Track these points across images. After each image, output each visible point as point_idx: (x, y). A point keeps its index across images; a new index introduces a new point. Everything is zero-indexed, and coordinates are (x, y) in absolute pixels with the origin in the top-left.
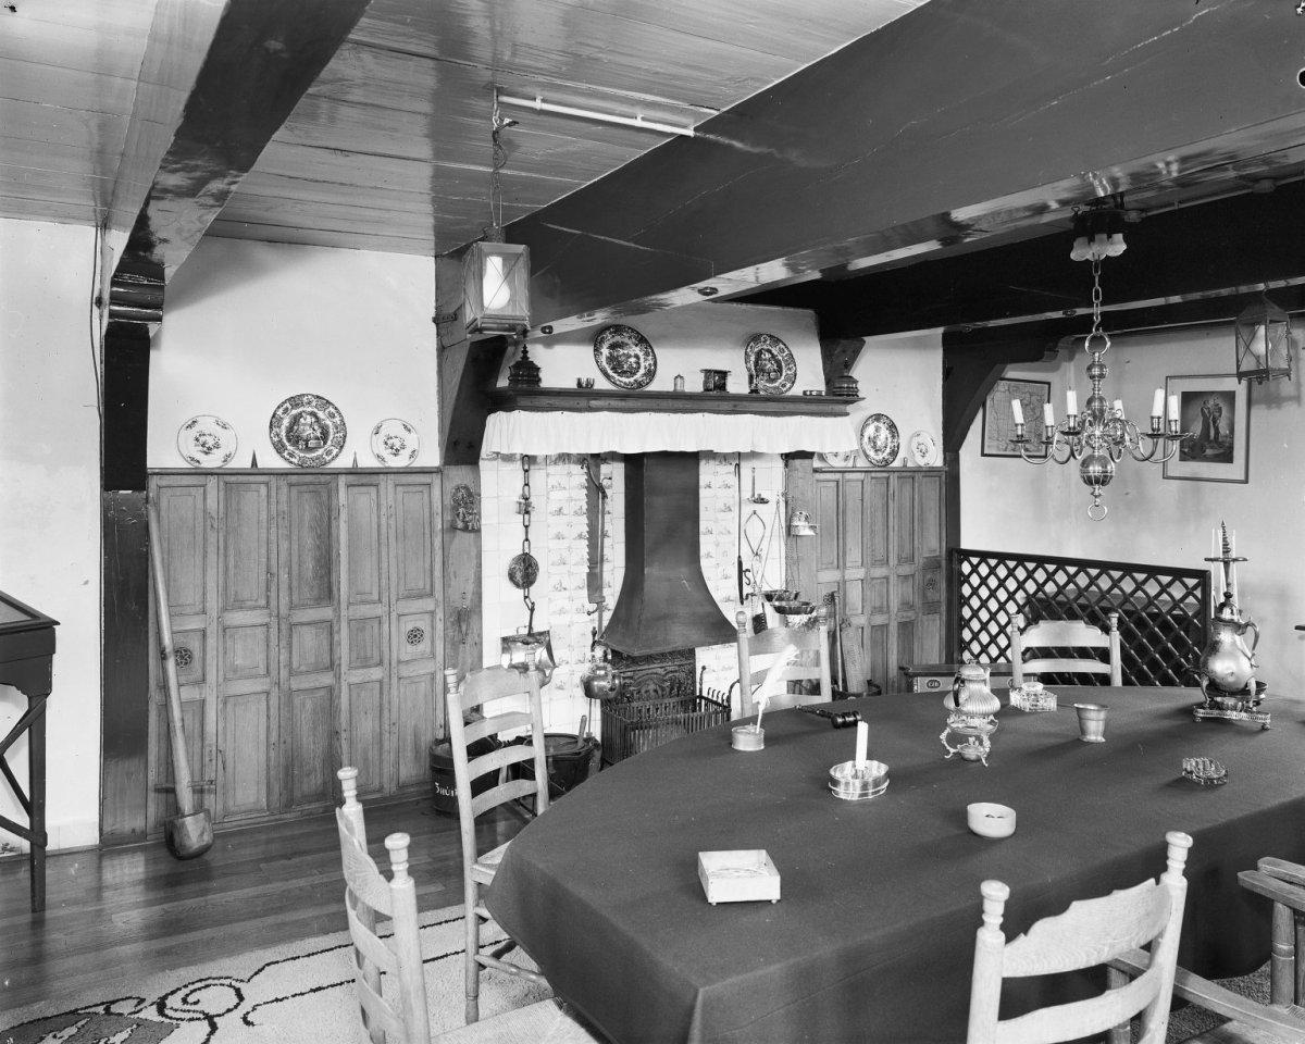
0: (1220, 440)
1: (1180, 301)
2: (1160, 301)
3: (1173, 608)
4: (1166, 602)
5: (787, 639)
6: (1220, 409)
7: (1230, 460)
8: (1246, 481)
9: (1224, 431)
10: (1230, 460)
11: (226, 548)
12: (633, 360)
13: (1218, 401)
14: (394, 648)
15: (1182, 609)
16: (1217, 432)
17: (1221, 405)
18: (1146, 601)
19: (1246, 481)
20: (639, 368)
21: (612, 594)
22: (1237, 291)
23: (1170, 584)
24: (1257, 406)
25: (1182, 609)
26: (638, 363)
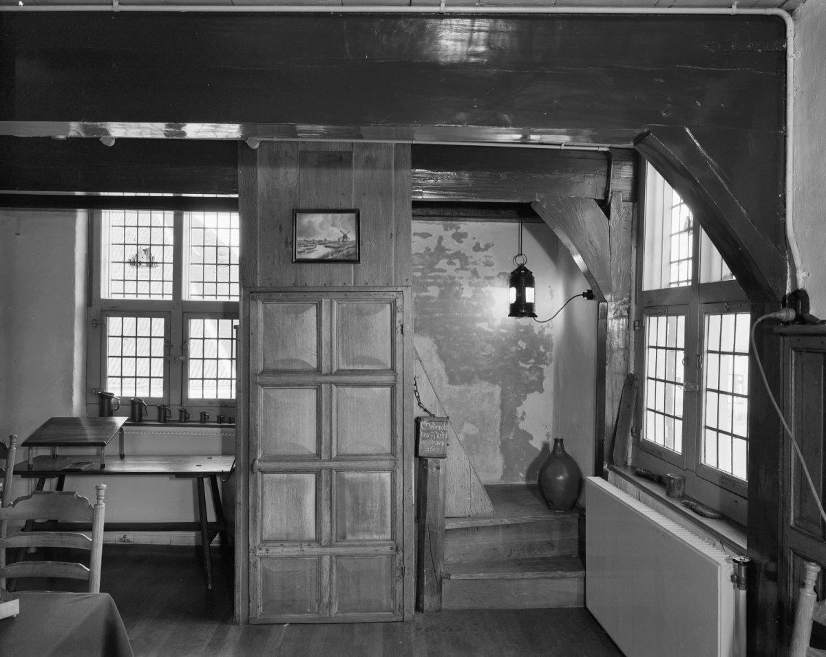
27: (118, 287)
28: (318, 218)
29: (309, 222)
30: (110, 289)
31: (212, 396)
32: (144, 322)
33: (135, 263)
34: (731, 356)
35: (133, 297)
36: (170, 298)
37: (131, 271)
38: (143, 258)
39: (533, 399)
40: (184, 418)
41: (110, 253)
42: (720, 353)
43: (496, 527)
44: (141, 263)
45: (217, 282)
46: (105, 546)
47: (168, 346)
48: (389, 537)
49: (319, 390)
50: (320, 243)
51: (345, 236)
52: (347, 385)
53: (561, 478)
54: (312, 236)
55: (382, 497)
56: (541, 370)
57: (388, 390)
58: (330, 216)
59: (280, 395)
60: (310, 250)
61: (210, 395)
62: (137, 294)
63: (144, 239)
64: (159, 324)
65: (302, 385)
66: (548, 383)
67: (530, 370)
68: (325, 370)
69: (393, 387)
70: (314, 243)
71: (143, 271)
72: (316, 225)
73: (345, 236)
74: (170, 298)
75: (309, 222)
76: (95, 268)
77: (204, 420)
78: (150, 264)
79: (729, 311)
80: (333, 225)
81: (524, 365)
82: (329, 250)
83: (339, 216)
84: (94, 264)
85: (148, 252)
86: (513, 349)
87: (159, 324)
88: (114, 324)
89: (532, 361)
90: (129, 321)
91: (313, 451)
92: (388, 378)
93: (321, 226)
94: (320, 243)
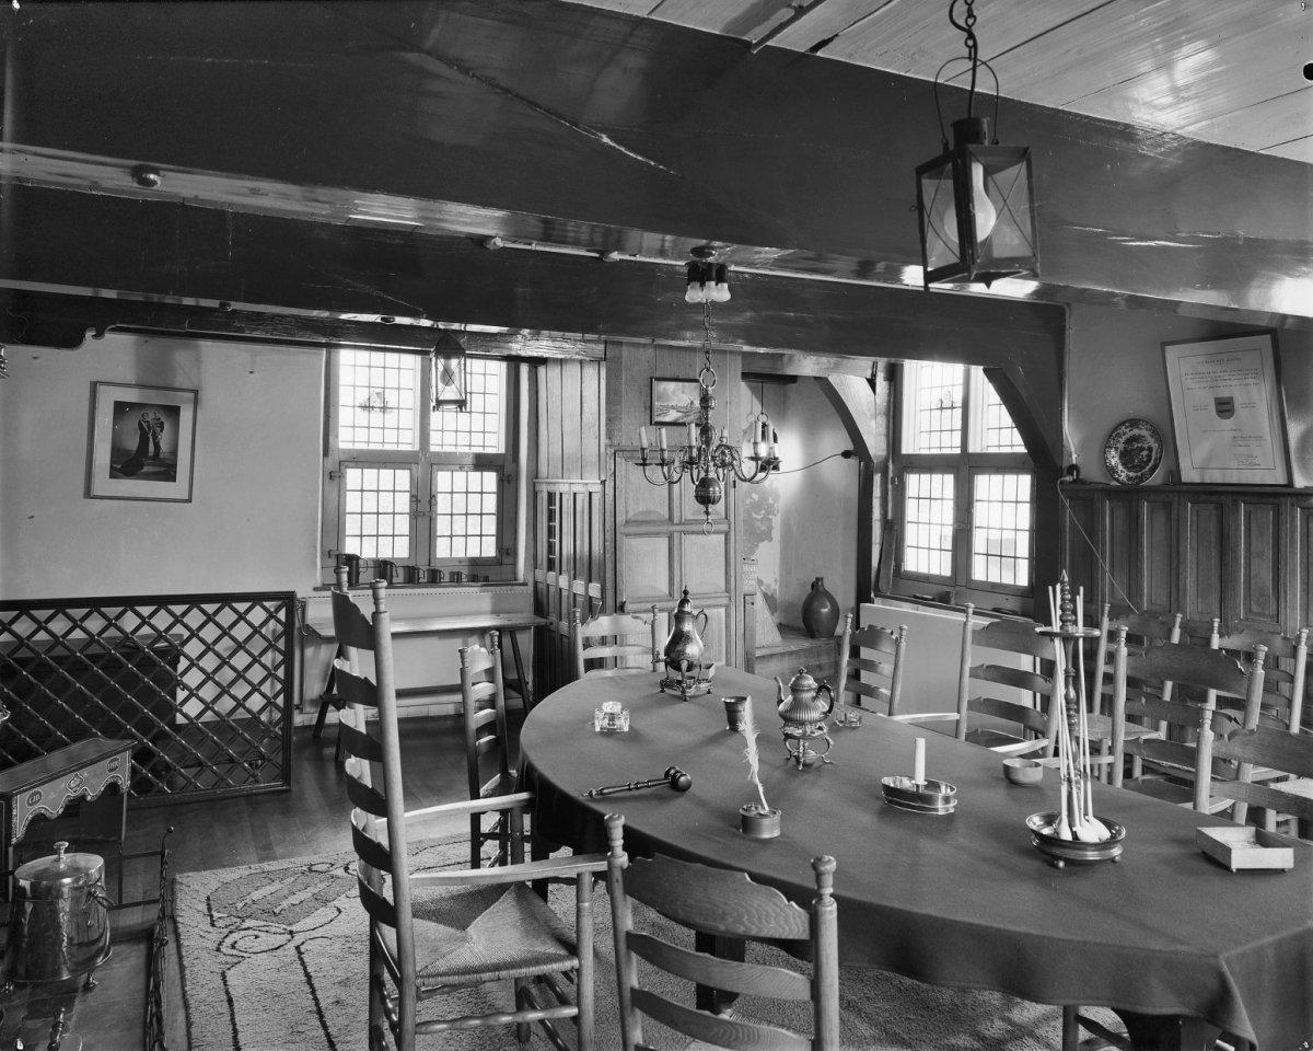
0: (161, 456)
1: (115, 297)
2: (87, 292)
3: (156, 640)
4: (43, 642)
5: (1252, 840)
6: (162, 426)
7: (173, 479)
8: (189, 501)
9: (164, 446)
10: (173, 479)
11: (922, 598)
12: (1145, 453)
13: (159, 415)
14: (468, 385)
15: (167, 641)
16: (157, 446)
17: (163, 419)
18: (156, 635)
19: (189, 501)
20: (1149, 461)
21: (1262, 152)
22: (198, 302)
23: (185, 614)
24: (1272, 305)
25: (167, 641)
26: (1149, 456)
27: (361, 435)
28: (671, 386)
29: (665, 389)
30: (348, 438)
31: (461, 555)
32: (386, 474)
33: (367, 407)
34: (986, 503)
35: (394, 447)
36: (958, 451)
37: (362, 416)
38: (376, 402)
39: (764, 546)
40: (434, 578)
41: (346, 397)
42: (989, 501)
43: (782, 654)
44: (373, 408)
45: (398, 429)
46: (400, 721)
47: (415, 499)
48: (724, 662)
49: (670, 538)
50: (673, 408)
51: (692, 403)
52: (693, 533)
53: (825, 610)
54: (668, 400)
55: (720, 630)
56: (770, 520)
57: (722, 537)
58: (681, 384)
59: (635, 542)
60: (665, 414)
61: (459, 553)
62: (941, 448)
63: (377, 381)
64: (403, 478)
65: (658, 534)
66: (776, 534)
67: (762, 520)
68: (676, 521)
69: (727, 534)
70: (668, 408)
71: (376, 416)
72: (670, 392)
73: (692, 403)
74: (958, 451)
75: (665, 389)
76: (332, 415)
77: (456, 579)
78: (384, 409)
79: (925, 472)
80: (683, 392)
81: (755, 516)
82: (680, 414)
83: (687, 384)
84: (332, 408)
85: (382, 395)
86: (748, 501)
87: (403, 478)
88: (353, 476)
89: (763, 512)
90: (370, 474)
91: (666, 590)
92: (724, 527)
93: (674, 392)
94: (673, 408)
